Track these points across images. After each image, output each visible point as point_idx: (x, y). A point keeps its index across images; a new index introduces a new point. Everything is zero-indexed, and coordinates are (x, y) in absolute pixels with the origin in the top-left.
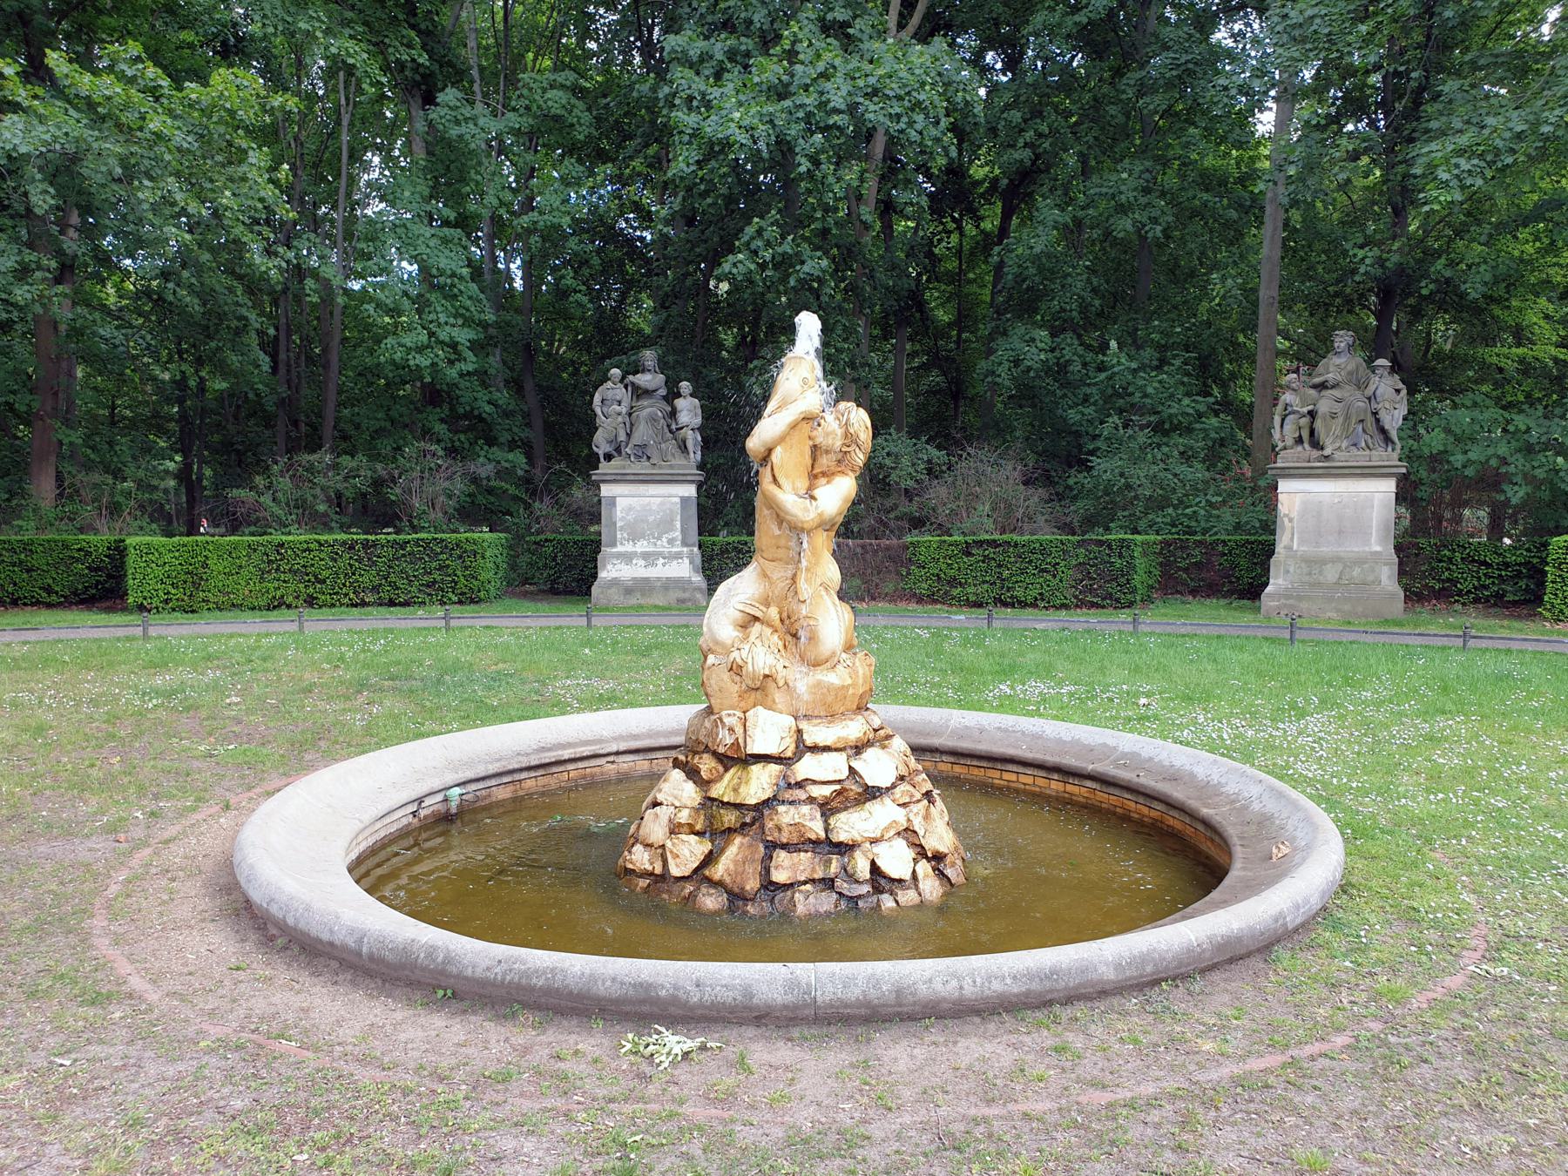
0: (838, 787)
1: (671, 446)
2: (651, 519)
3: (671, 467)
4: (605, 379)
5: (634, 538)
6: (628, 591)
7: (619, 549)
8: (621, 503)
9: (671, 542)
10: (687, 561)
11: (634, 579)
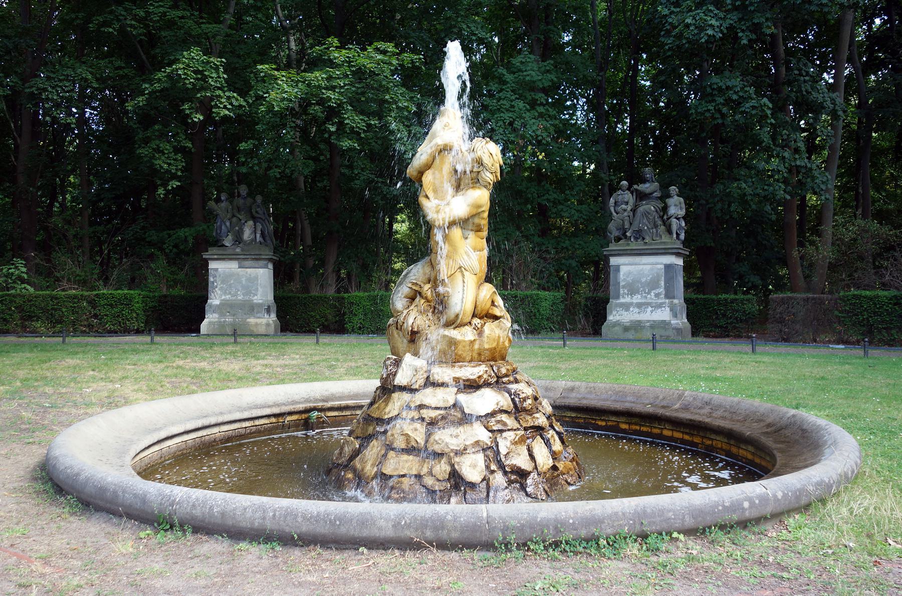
0: (442, 412)
2: (643, 280)
3: (656, 244)
5: (632, 292)
6: (626, 329)
7: (622, 300)
8: (624, 270)
9: (657, 295)
10: (668, 309)
11: (631, 321)
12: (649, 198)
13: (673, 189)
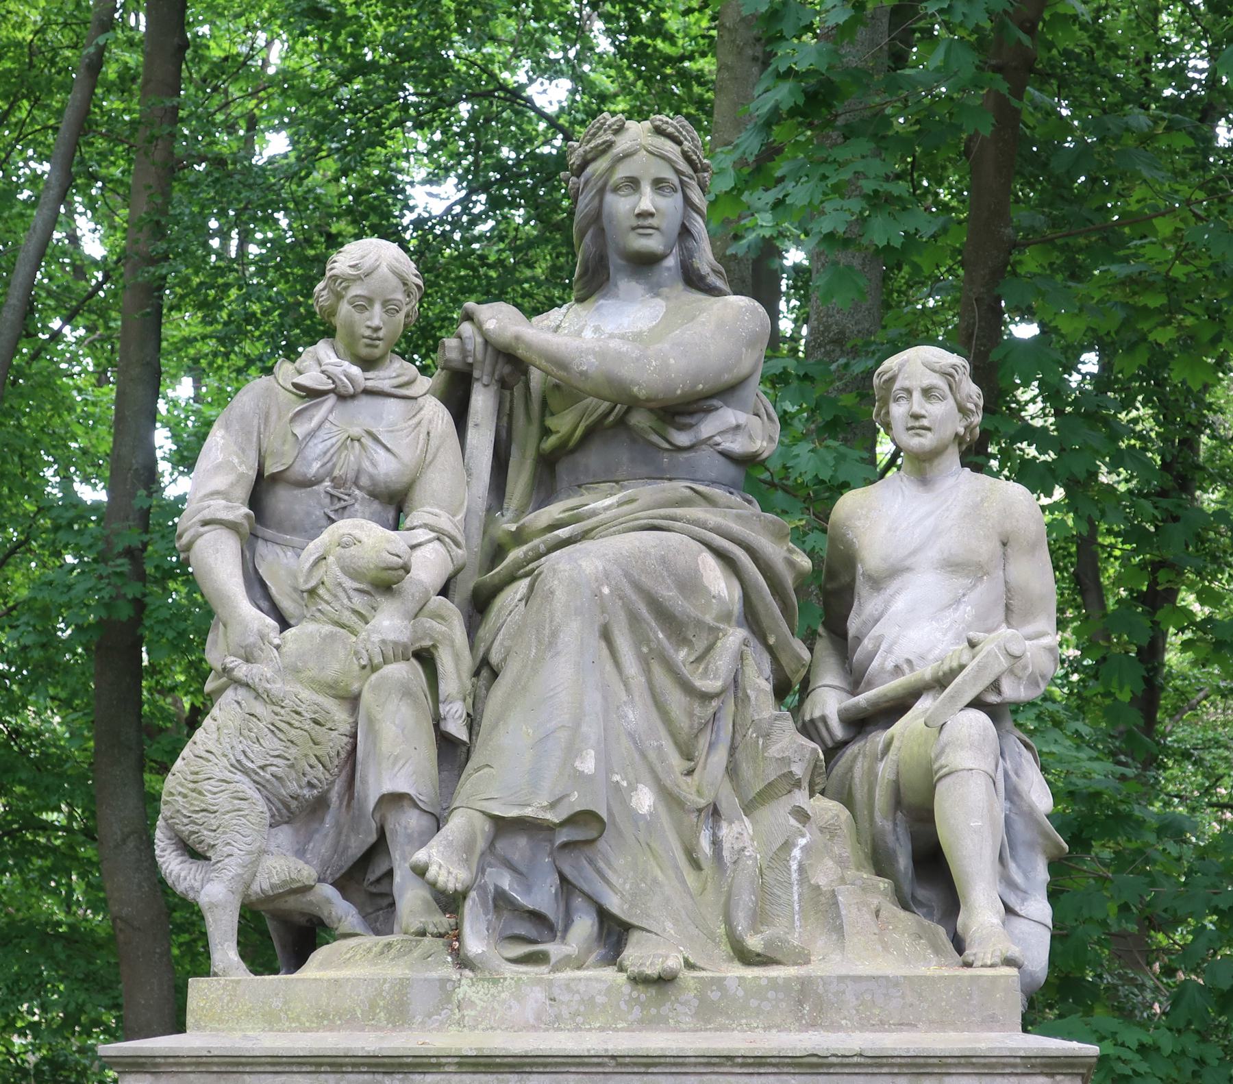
1: (811, 842)
3: (808, 1001)
4: (155, 428)
12: (653, 461)
13: (926, 379)
